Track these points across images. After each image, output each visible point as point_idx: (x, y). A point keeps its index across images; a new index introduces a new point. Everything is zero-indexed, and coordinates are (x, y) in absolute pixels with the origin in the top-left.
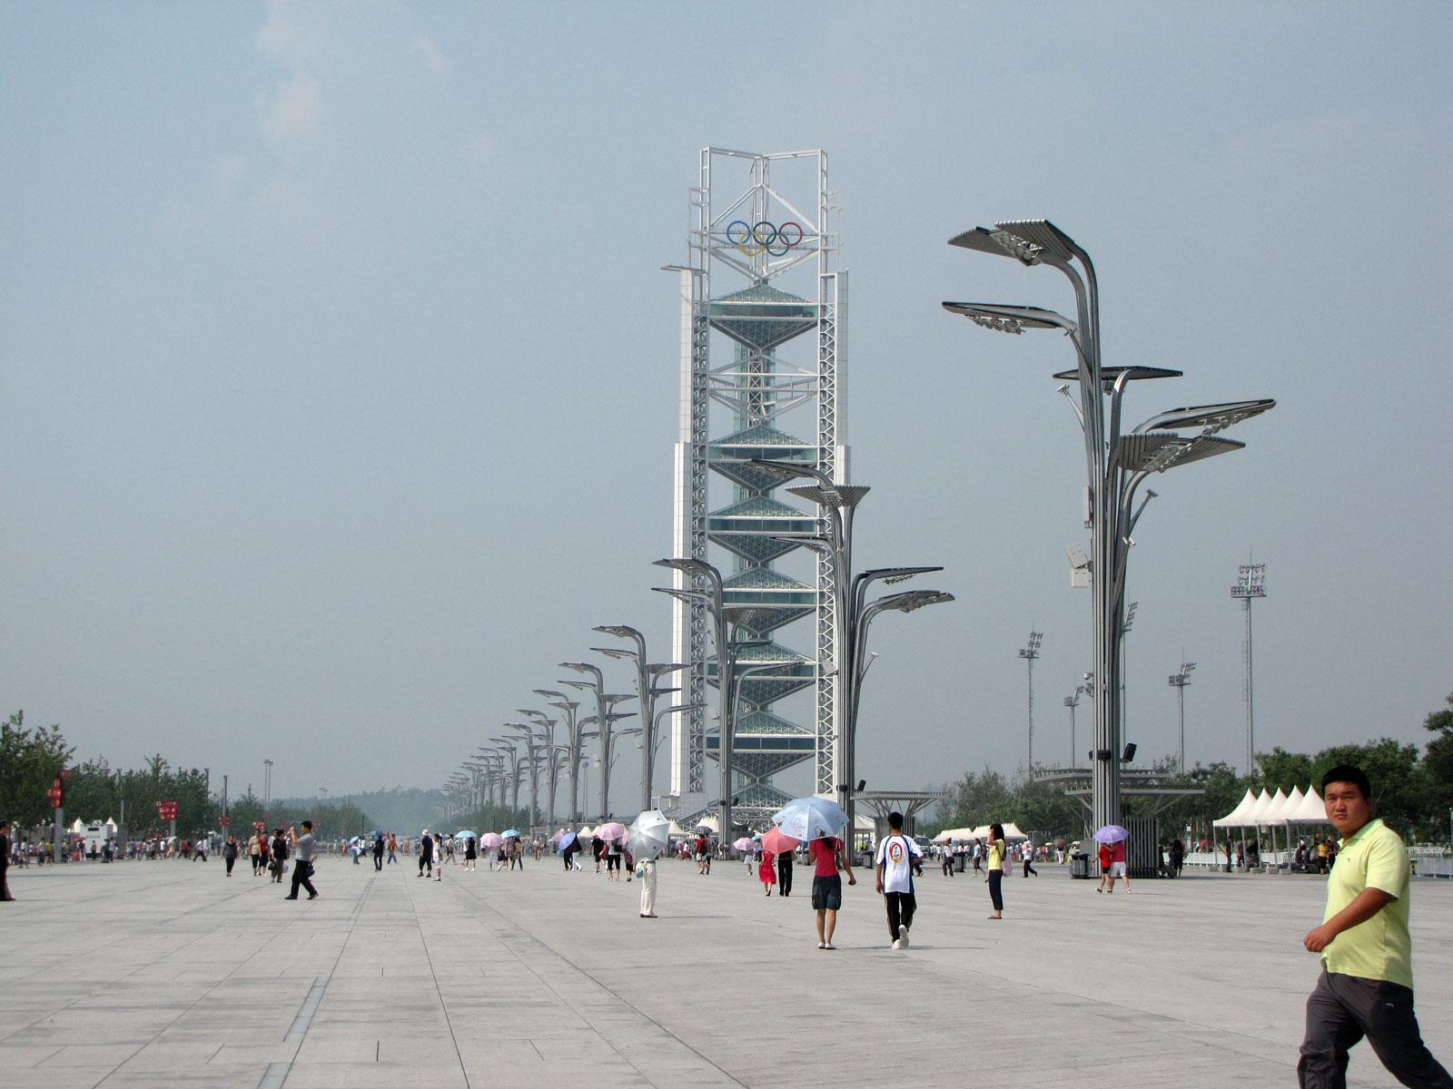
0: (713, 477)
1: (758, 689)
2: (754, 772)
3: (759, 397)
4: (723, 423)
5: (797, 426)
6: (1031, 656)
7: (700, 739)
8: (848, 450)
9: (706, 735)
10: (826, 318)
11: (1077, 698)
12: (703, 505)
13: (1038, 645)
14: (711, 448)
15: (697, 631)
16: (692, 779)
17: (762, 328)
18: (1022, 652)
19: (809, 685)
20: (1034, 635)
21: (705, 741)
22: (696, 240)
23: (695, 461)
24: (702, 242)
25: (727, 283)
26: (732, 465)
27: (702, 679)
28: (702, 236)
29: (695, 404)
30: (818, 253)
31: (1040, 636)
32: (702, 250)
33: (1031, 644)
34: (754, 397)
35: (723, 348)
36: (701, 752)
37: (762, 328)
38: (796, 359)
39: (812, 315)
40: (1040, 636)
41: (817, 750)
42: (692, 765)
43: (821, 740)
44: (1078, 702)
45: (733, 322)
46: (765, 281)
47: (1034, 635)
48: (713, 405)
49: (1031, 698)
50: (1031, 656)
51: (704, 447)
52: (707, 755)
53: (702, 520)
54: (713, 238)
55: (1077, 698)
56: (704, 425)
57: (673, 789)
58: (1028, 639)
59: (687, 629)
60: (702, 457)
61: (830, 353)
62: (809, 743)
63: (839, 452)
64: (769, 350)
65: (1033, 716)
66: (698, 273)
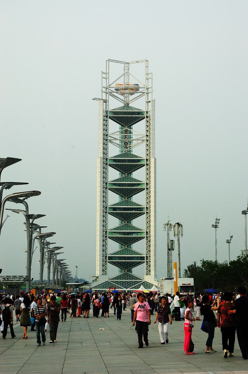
0: (109, 241)
1: (126, 240)
2: (125, 268)
3: (127, 144)
4: (114, 151)
5: (139, 151)
6: (216, 227)
7: (106, 257)
8: (155, 159)
9: (108, 256)
10: (148, 163)
11: (231, 240)
12: (107, 227)
13: (218, 223)
14: (109, 183)
15: (105, 240)
16: (103, 270)
17: (127, 118)
18: (213, 225)
19: (143, 263)
20: (217, 219)
21: (107, 257)
22: (104, 90)
23: (104, 163)
24: (106, 91)
25: (115, 104)
26: (116, 165)
27: (106, 261)
28: (106, 89)
29: (104, 121)
30: (145, 93)
31: (219, 220)
32: (106, 93)
33: (216, 223)
34: (126, 143)
35: (114, 127)
36: (106, 261)
37: (127, 118)
38: (139, 129)
39: (143, 114)
40: (219, 220)
41: (145, 261)
42: (103, 266)
43: (147, 257)
44: (231, 241)
45: (117, 117)
46: (128, 104)
47: (217, 219)
48: (110, 145)
49: (216, 242)
50: (216, 227)
51: (107, 140)
52: (108, 262)
53: (106, 208)
54: (110, 90)
55: (231, 240)
56: (107, 152)
57: (97, 274)
58: (215, 221)
59: (102, 181)
60: (107, 163)
61: (149, 146)
62: (143, 258)
63: (152, 160)
64: (130, 127)
65: (217, 248)
66: (105, 101)
